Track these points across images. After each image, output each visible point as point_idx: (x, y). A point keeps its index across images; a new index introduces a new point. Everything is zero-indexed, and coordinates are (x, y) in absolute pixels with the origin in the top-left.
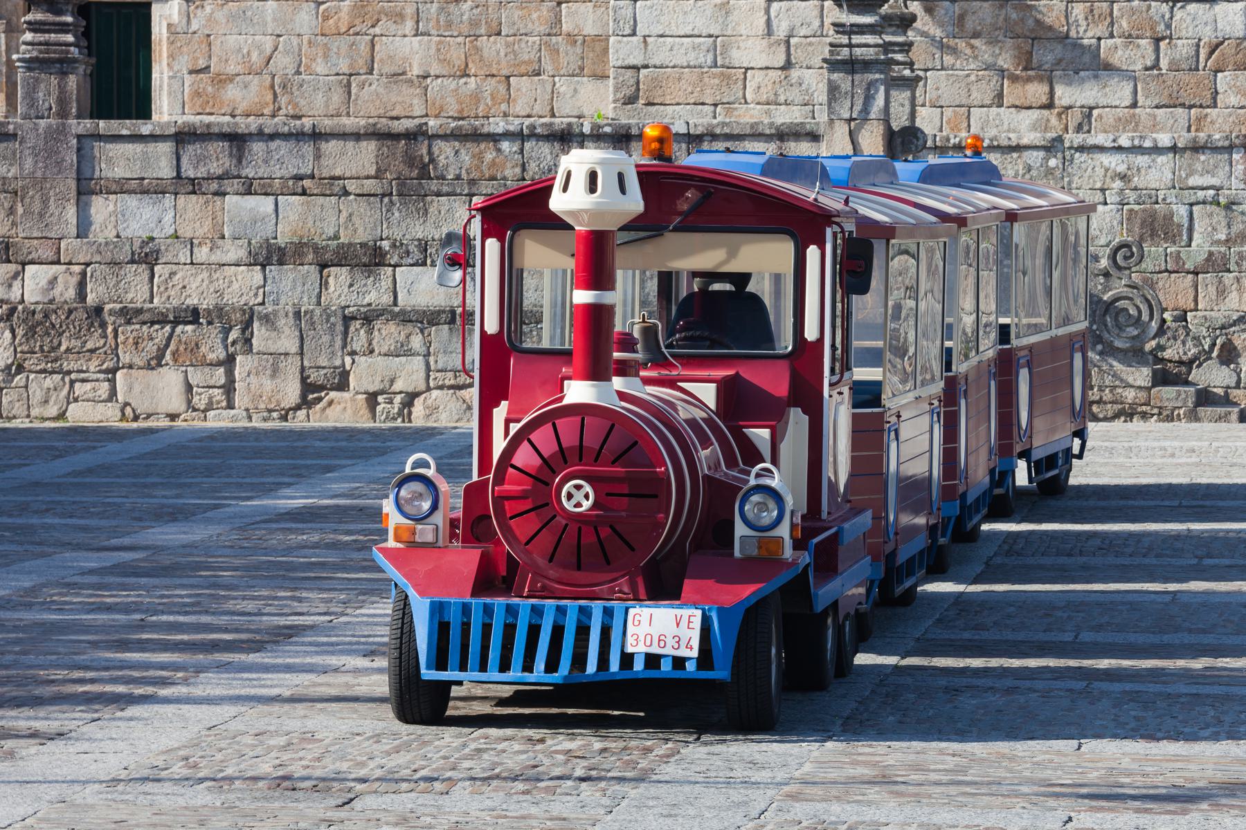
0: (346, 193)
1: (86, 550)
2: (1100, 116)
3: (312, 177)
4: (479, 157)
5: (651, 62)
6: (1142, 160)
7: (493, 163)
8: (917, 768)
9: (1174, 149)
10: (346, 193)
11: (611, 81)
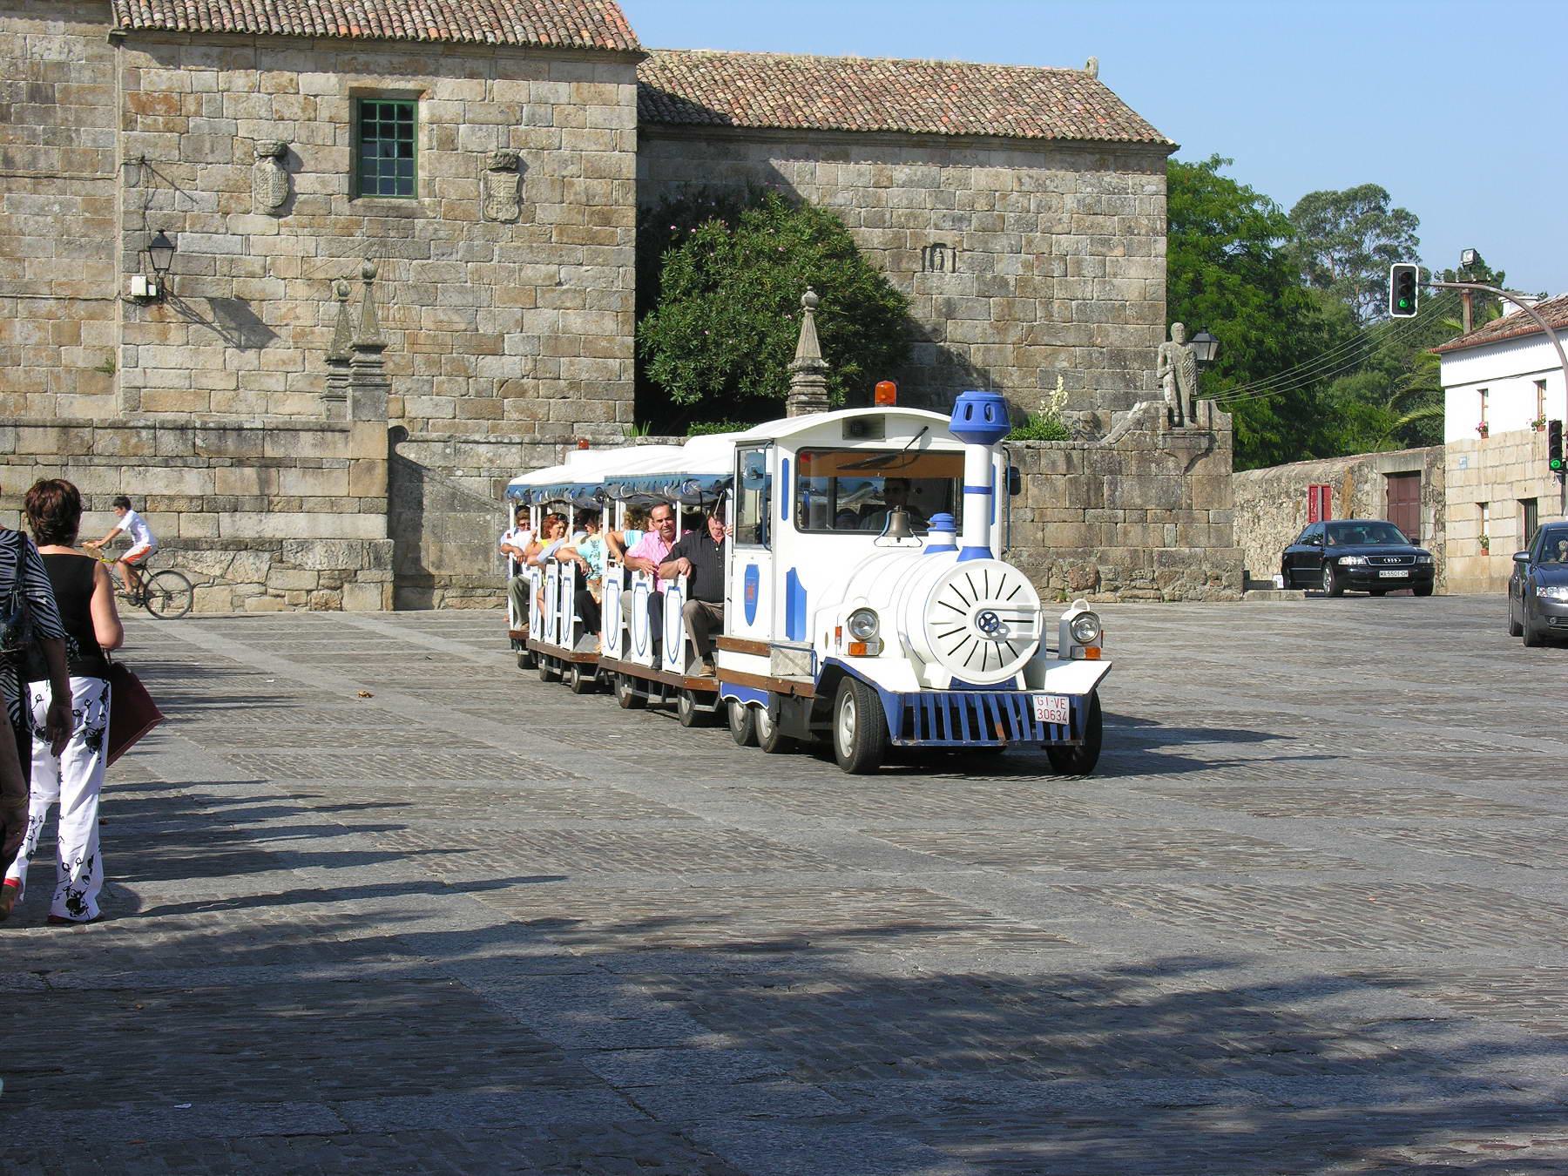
0: (37, 463)
1: (1375, 985)
2: (434, 424)
3: (14, 453)
4: (126, 442)
5: (149, 385)
6: (503, 450)
7: (136, 446)
8: (709, 893)
9: (521, 443)
10: (37, 463)
11: (349, 402)
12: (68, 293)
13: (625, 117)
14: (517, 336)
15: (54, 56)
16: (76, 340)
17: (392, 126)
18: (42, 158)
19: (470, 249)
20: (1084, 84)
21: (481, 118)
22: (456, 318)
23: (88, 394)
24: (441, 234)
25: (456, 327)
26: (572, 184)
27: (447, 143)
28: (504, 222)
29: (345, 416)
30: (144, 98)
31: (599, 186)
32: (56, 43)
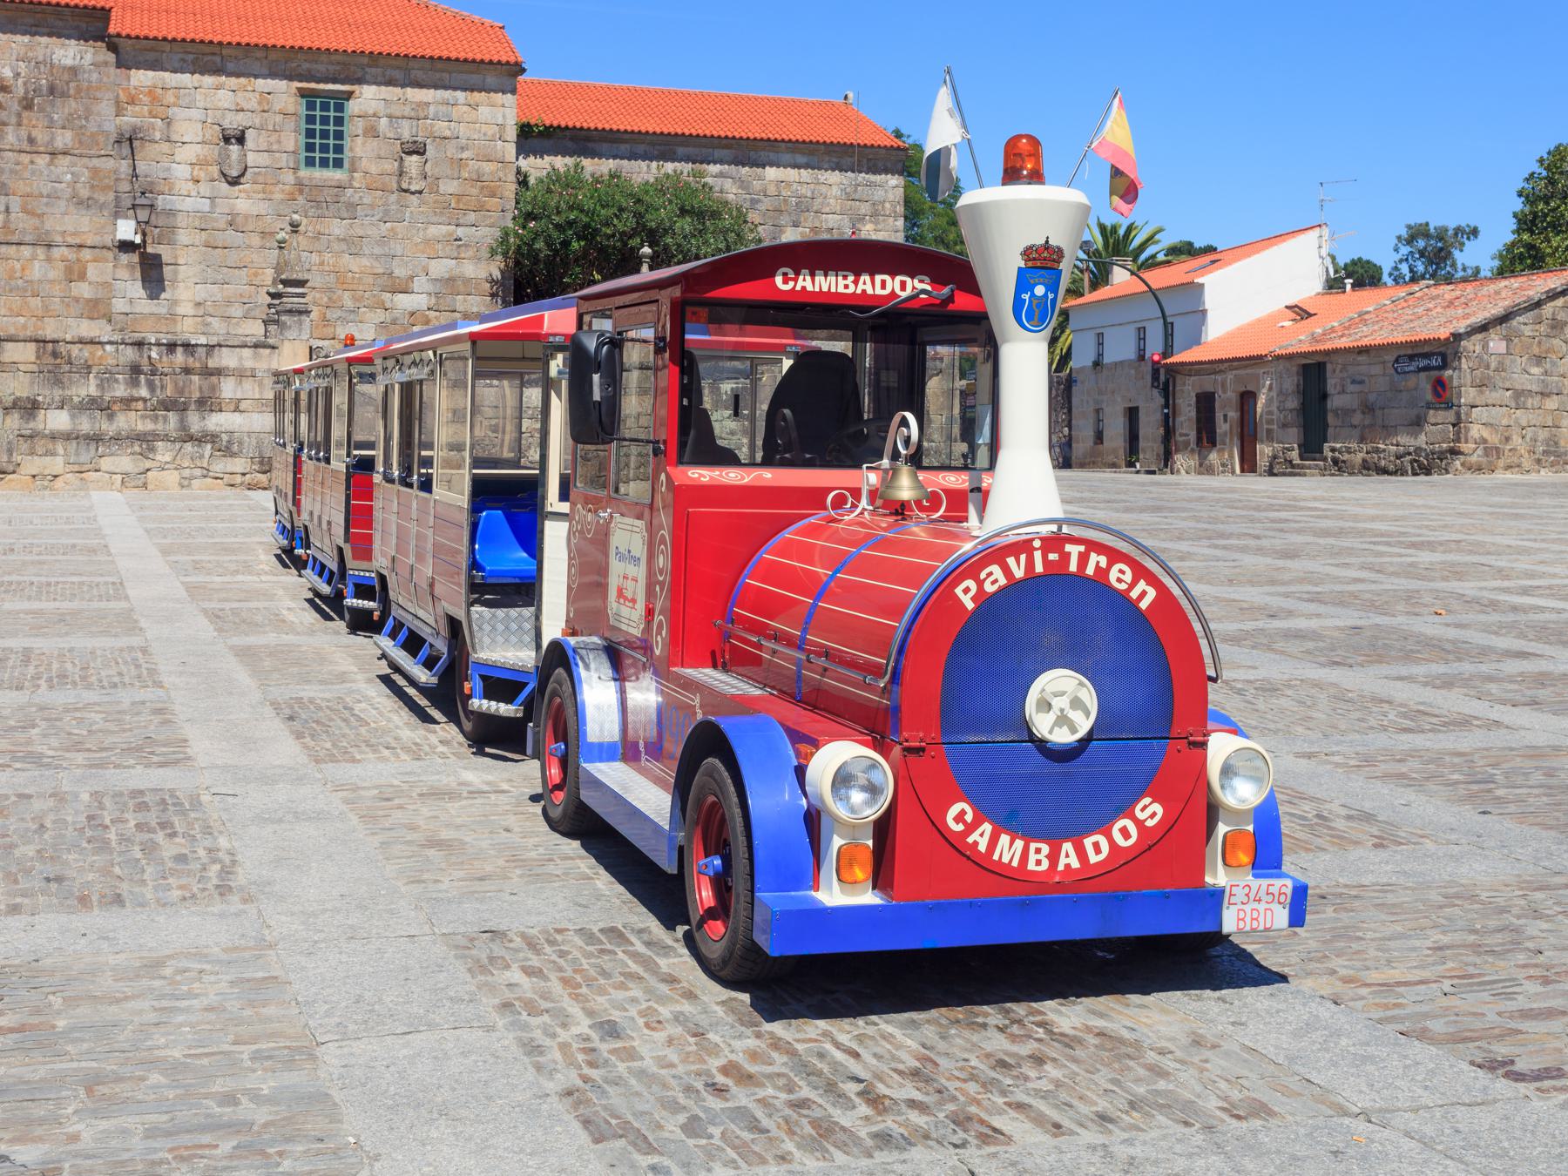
12: (78, 241)
13: (508, 116)
14: (424, 279)
15: (69, 62)
16: (82, 276)
17: (314, 151)
18: (59, 138)
19: (386, 212)
20: (840, 112)
21: (398, 114)
22: (376, 264)
23: (92, 319)
24: (365, 201)
25: (376, 271)
26: (467, 165)
27: (372, 132)
28: (413, 193)
29: (975, 354)
30: (133, 92)
31: (488, 168)
32: (71, 52)
